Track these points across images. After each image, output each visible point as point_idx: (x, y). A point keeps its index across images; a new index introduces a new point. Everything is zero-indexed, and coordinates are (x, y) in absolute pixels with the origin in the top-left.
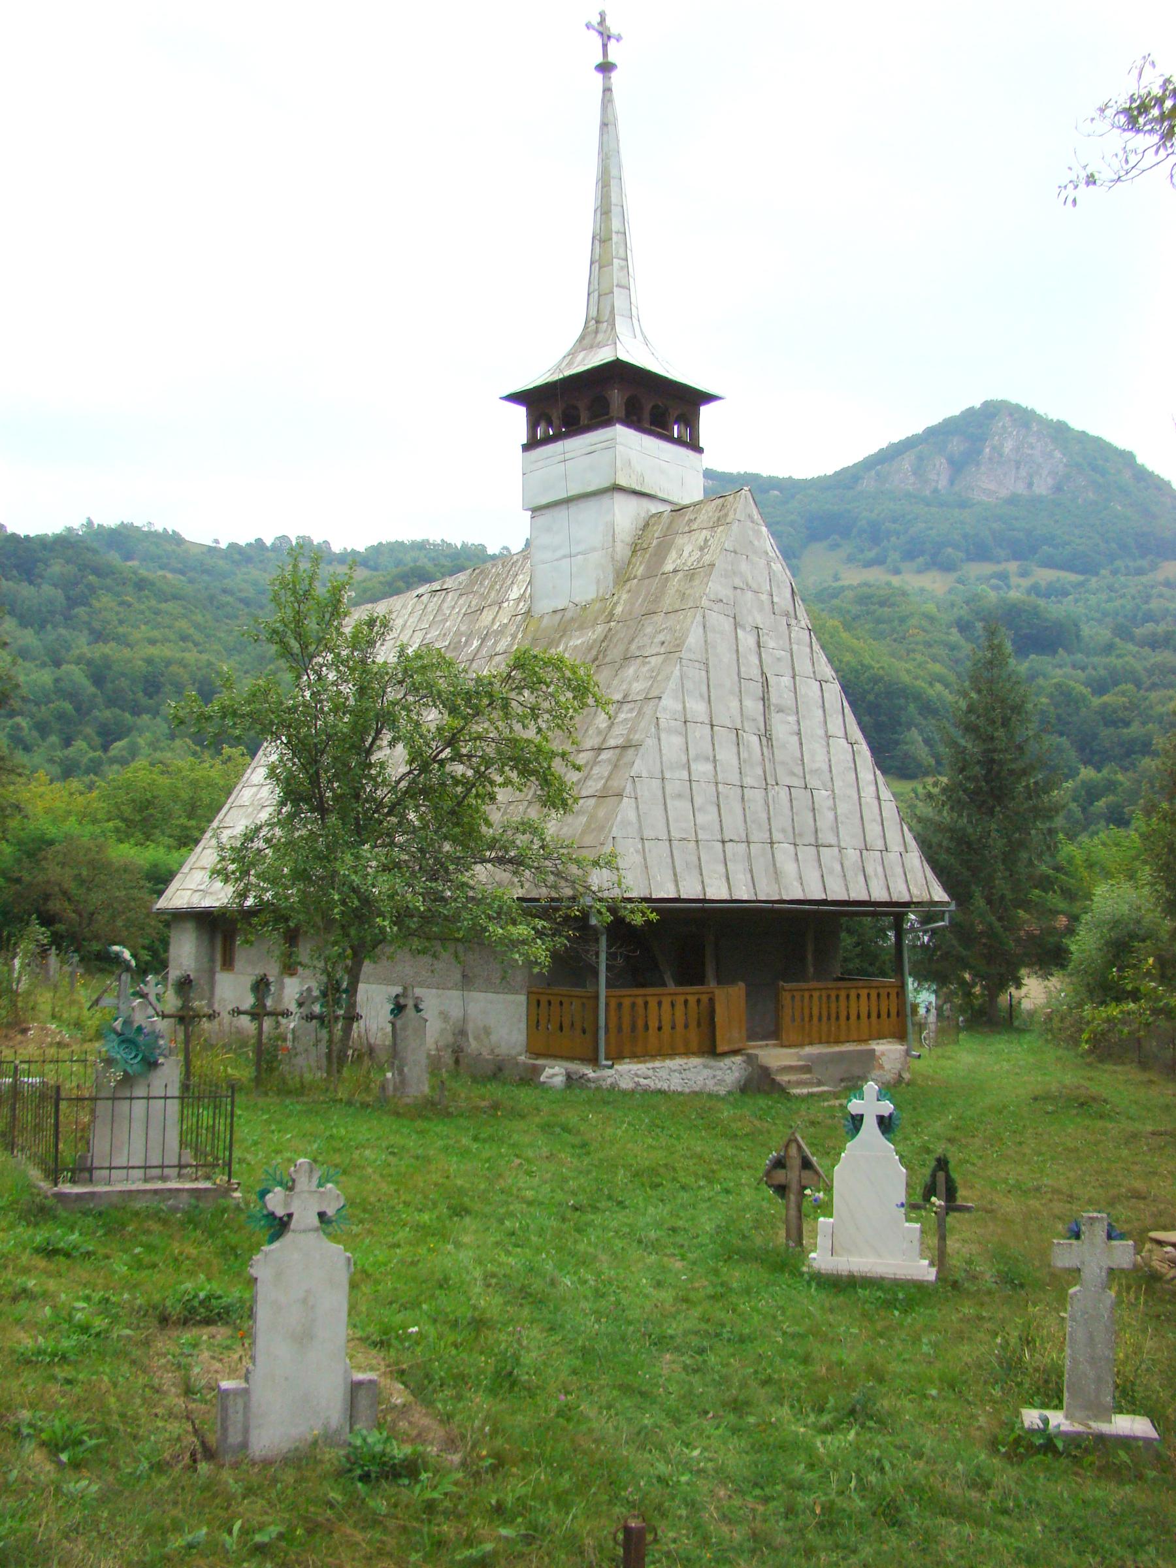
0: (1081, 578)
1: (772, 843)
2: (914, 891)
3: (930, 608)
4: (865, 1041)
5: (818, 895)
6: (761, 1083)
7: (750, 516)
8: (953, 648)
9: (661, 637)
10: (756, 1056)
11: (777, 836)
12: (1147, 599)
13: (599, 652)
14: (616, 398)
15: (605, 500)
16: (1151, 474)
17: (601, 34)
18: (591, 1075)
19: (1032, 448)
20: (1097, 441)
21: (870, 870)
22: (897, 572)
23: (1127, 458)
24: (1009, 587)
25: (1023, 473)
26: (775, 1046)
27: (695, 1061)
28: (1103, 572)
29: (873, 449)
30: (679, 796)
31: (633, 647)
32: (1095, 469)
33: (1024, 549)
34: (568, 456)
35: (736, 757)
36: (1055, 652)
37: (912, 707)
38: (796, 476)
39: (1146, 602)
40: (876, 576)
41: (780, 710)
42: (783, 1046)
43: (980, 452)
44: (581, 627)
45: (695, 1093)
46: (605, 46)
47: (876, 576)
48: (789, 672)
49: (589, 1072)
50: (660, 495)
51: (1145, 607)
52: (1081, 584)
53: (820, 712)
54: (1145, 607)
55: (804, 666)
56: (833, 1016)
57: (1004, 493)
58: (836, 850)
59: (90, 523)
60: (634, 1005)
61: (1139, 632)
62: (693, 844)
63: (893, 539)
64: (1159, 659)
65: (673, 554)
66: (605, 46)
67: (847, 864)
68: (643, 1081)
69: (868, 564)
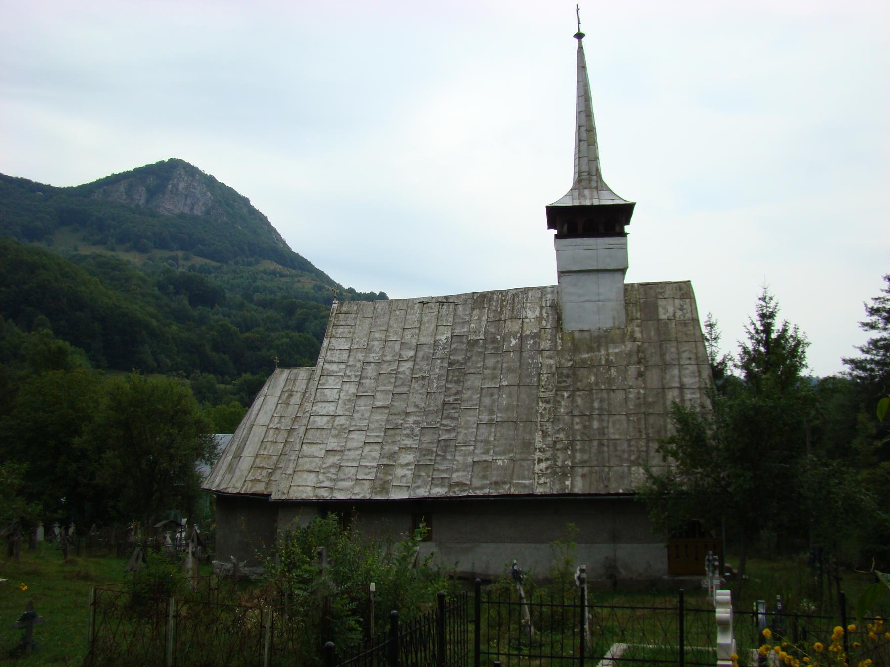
0: (219, 264)
3: (142, 274)
16: (257, 212)
20: (231, 189)
23: (246, 201)
25: (189, 201)
29: (103, 176)
36: (212, 307)
38: (53, 185)
40: (99, 250)
44: (613, 342)
47: (99, 250)
52: (219, 268)
57: (177, 211)
69: (95, 243)
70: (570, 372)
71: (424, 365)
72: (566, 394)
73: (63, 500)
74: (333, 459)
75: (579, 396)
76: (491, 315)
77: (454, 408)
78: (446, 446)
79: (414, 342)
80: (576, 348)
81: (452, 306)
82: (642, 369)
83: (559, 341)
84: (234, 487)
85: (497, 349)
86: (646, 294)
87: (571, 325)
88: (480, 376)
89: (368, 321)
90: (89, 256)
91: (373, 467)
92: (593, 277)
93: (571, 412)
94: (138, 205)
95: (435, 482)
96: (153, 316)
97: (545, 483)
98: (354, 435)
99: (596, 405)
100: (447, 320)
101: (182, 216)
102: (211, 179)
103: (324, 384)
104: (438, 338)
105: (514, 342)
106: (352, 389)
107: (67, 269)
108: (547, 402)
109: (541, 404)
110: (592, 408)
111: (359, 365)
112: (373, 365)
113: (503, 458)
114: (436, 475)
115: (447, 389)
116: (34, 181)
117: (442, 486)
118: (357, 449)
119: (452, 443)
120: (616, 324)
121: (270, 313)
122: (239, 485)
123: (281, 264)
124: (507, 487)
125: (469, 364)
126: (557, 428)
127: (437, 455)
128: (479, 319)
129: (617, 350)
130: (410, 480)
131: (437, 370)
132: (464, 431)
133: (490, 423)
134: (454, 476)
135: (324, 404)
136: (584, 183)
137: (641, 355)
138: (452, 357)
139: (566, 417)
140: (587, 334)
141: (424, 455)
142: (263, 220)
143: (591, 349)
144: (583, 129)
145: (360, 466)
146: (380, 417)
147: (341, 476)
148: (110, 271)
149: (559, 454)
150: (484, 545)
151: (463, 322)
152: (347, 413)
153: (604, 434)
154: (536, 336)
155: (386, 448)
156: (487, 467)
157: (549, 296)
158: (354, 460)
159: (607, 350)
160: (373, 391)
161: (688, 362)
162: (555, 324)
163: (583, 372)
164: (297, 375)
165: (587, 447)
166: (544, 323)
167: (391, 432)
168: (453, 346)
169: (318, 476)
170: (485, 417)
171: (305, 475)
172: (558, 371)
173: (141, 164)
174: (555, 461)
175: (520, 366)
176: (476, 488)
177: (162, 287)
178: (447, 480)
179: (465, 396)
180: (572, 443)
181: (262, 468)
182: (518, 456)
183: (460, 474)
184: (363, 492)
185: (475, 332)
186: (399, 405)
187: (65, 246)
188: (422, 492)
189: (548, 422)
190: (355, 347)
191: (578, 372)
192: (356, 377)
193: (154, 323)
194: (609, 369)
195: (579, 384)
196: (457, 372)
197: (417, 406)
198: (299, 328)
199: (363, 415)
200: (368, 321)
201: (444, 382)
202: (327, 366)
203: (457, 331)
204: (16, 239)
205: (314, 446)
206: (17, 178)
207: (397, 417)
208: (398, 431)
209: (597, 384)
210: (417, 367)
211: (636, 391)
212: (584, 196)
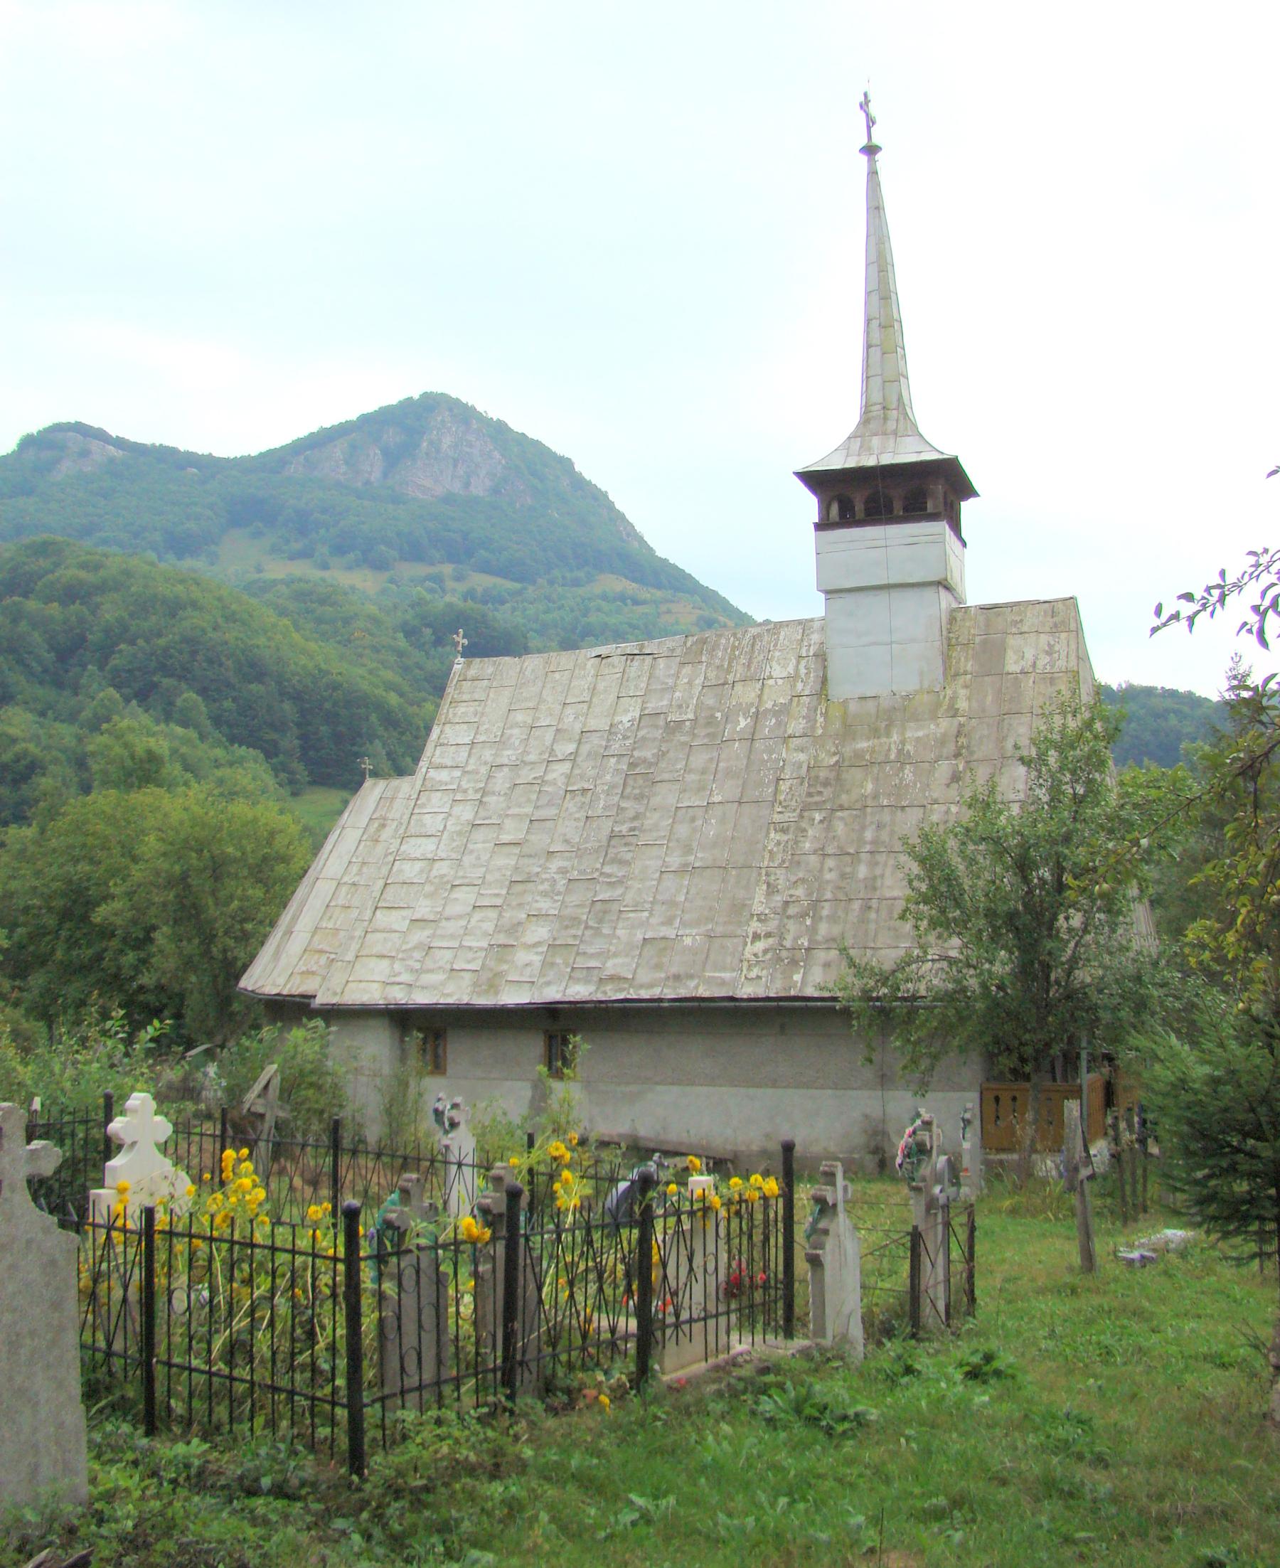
0: (518, 586)
3: (372, 609)
8: (401, 654)
15: (929, 593)
19: (471, 446)
20: (537, 444)
22: (325, 566)
24: (443, 590)
28: (540, 581)
29: (303, 432)
33: (461, 551)
37: (373, 718)
38: (217, 454)
39: (585, 616)
40: (301, 569)
44: (915, 718)
52: (519, 593)
59: (1240, 682)
63: (322, 531)
70: (832, 775)
71: (588, 768)
72: (818, 817)
74: (420, 935)
75: (842, 819)
76: (712, 674)
77: (626, 844)
78: (603, 911)
79: (578, 727)
80: (848, 730)
81: (649, 659)
82: (961, 768)
83: (820, 720)
84: (274, 985)
85: (711, 736)
86: (987, 625)
87: (838, 691)
88: (677, 786)
89: (507, 693)
90: (282, 581)
91: (481, 949)
92: (884, 595)
93: (822, 849)
94: (367, 483)
95: (577, 974)
96: (390, 687)
97: (759, 977)
98: (459, 894)
99: (868, 835)
100: (636, 687)
101: (449, 499)
103: (423, 806)
104: (617, 719)
105: (743, 723)
107: (234, 607)
108: (784, 831)
109: (772, 835)
110: (861, 841)
111: (484, 770)
112: (506, 769)
113: (694, 932)
114: (581, 962)
115: (621, 810)
117: (587, 981)
118: (460, 917)
119: (615, 907)
120: (926, 685)
122: (281, 981)
124: (692, 984)
125: (663, 765)
126: (793, 879)
127: (586, 928)
128: (690, 683)
129: (920, 734)
130: (537, 972)
131: (608, 777)
132: (637, 885)
133: (683, 870)
134: (610, 964)
135: (420, 840)
136: (872, 426)
137: (962, 740)
138: (636, 754)
139: (813, 858)
140: (871, 705)
141: (567, 927)
142: (598, 498)
143: (875, 733)
144: (875, 324)
145: (461, 946)
146: (505, 861)
147: (429, 964)
148: (314, 606)
149: (792, 926)
150: (659, 1088)
151: (663, 690)
152: (454, 856)
153: (875, 889)
154: (782, 711)
155: (507, 915)
156: (665, 949)
157: (815, 638)
158: (453, 937)
159: (903, 734)
160: (500, 816)
162: (818, 687)
163: (857, 774)
164: (397, 790)
165: (840, 913)
166: (800, 686)
167: (519, 887)
168: (641, 734)
169: (392, 965)
170: (675, 861)
171: (373, 962)
172: (811, 778)
173: (370, 407)
174: (782, 938)
175: (747, 766)
176: (641, 986)
177: (410, 632)
178: (596, 972)
179: (648, 823)
180: (816, 904)
181: (321, 952)
182: (720, 930)
183: (619, 960)
184: (458, 993)
185: (680, 706)
186: (539, 840)
187: (240, 568)
189: (780, 866)
190: (481, 738)
191: (844, 776)
192: (476, 791)
193: (393, 699)
194: (902, 769)
195: (844, 797)
196: (640, 777)
197: (567, 841)
199: (478, 858)
200: (507, 693)
201: (617, 798)
202: (432, 773)
203: (651, 706)
204: (152, 556)
205: (394, 912)
207: (531, 861)
208: (530, 886)
209: (875, 796)
210: (577, 771)
211: (943, 808)
212: (869, 449)
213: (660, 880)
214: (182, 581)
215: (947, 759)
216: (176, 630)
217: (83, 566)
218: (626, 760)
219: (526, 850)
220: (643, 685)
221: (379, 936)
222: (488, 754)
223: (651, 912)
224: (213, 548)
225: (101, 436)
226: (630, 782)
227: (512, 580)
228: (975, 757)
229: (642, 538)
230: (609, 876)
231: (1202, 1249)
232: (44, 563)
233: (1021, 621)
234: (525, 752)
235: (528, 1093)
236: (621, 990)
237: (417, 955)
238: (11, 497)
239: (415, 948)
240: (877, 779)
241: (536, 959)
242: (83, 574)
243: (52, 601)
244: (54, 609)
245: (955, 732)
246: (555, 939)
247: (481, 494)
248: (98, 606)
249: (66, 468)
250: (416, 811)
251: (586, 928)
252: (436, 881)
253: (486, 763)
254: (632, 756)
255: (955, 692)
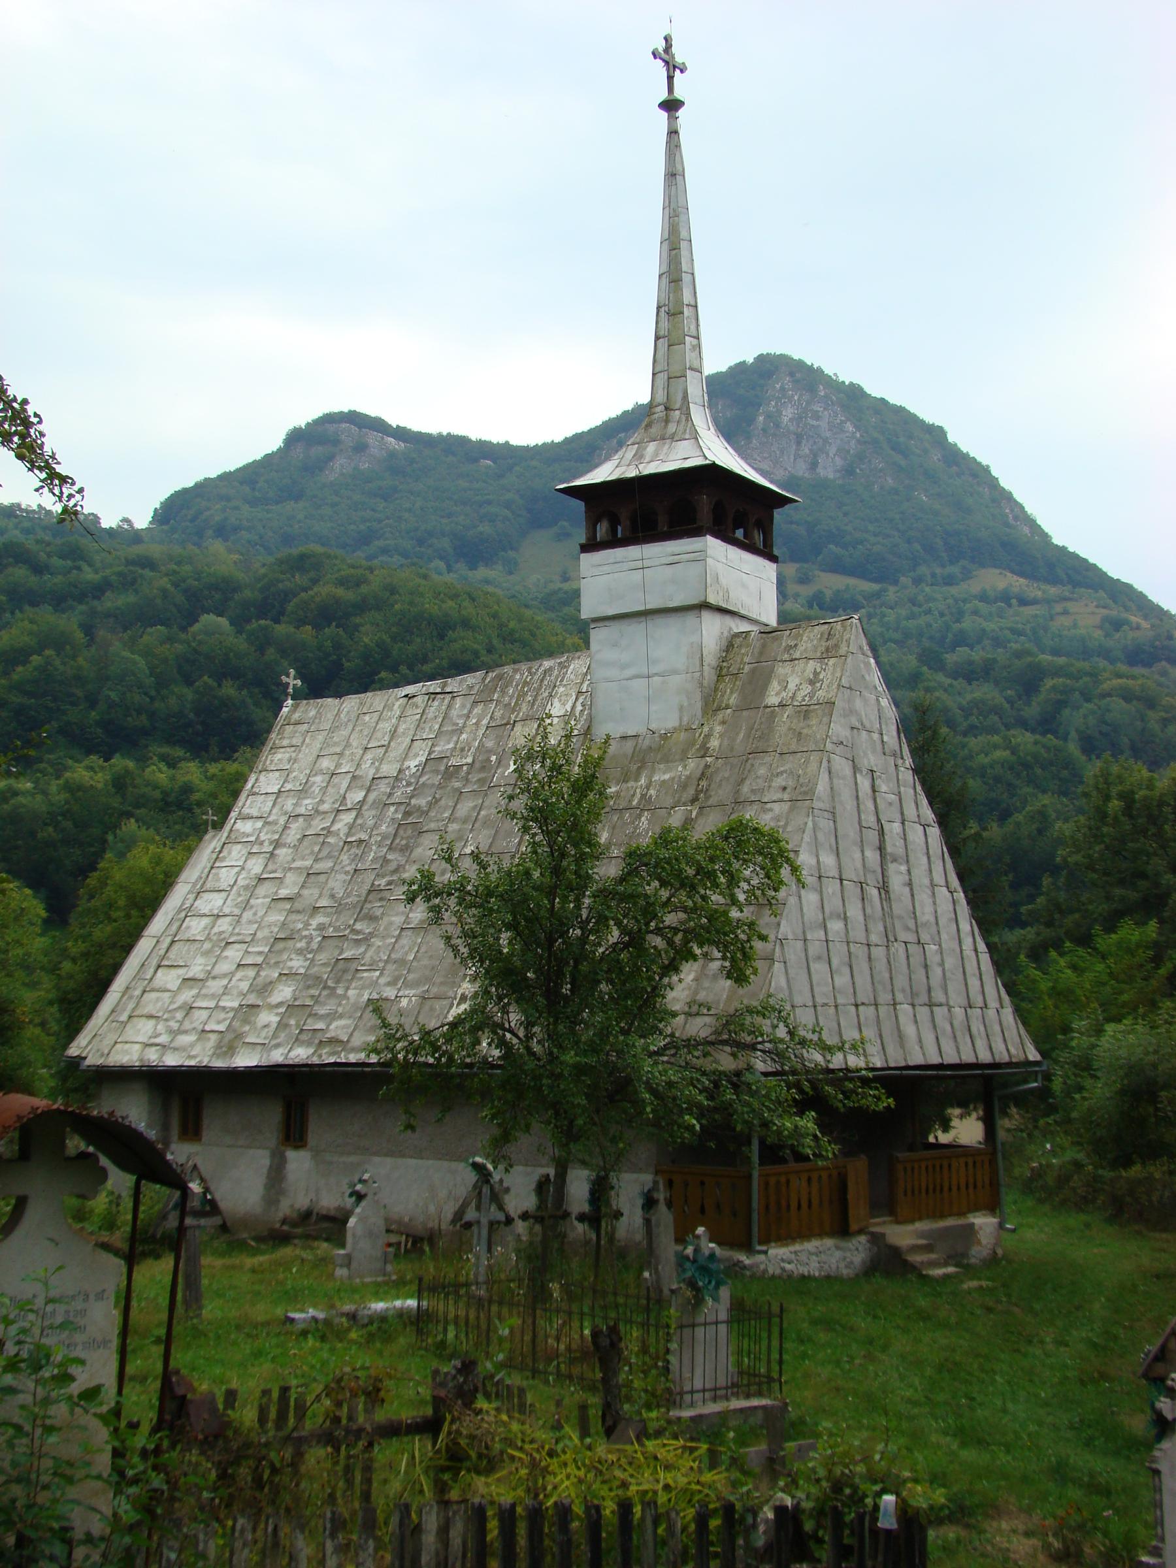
0: (875, 587)
1: (895, 1004)
2: (1013, 1051)
4: (962, 1214)
5: (935, 1060)
6: (889, 1263)
7: (861, 648)
9: (780, 781)
10: (883, 1235)
11: (900, 997)
12: (959, 616)
13: (698, 792)
14: (704, 503)
15: (691, 619)
16: (966, 457)
17: (667, 63)
18: (747, 1262)
19: (818, 418)
20: (900, 411)
21: (974, 1029)
23: (936, 434)
25: (806, 450)
26: (891, 1222)
27: (829, 1242)
28: (903, 579)
29: (614, 411)
30: (819, 958)
31: (745, 789)
32: (896, 448)
34: (646, 563)
35: (861, 913)
38: (514, 442)
39: (958, 621)
41: (895, 860)
42: (898, 1222)
43: (751, 421)
44: (666, 760)
45: (828, 1277)
46: (670, 79)
48: (898, 817)
49: (746, 1260)
50: (743, 612)
51: (956, 626)
52: (878, 595)
53: (925, 859)
54: (956, 626)
55: (910, 811)
56: (938, 1188)
58: (945, 1009)
60: (778, 1182)
61: (951, 658)
62: (832, 1010)
64: (977, 695)
65: (775, 685)
66: (670, 79)
67: (956, 1023)
68: (788, 1267)
73: (1048, 1146)
74: (187, 995)
77: (381, 899)
78: (344, 970)
81: (448, 697)
82: (694, 814)
89: (321, 737)
91: (232, 1009)
95: (304, 1037)
102: (854, 393)
106: (256, 866)
107: (512, 624)
112: (301, 819)
113: (412, 992)
115: (386, 861)
116: (474, 437)
117: (308, 1044)
119: (354, 966)
121: (983, 692)
123: (1021, 574)
129: (667, 777)
137: (704, 783)
140: (630, 744)
142: (979, 474)
146: (276, 917)
150: (377, 1159)
155: (263, 974)
161: (779, 796)
167: (281, 945)
182: (435, 990)
183: (342, 1022)
186: (310, 893)
188: (277, 1056)
190: (288, 786)
198: (1047, 724)
199: (255, 914)
200: (321, 737)
206: (440, 435)
208: (290, 943)
210: (359, 821)
213: (398, 937)
214: (454, 597)
215: (684, 804)
216: (443, 654)
217: (342, 582)
218: (402, 808)
219: (298, 905)
220: (437, 727)
221: (154, 995)
222: (289, 804)
223: (383, 970)
224: (511, 553)
225: (378, 425)
226: (401, 832)
227: (870, 580)
228: (709, 803)
229: (1034, 521)
230: (358, 932)
231: (1047, 1355)
232: (299, 579)
233: (796, 645)
234: (322, 801)
235: (267, 1162)
236: (338, 1053)
237: (179, 1015)
238: (277, 503)
239: (179, 1008)
240: (614, 828)
241: (275, 1019)
242: (340, 592)
243: (305, 624)
244: (307, 633)
245: (698, 773)
246: (295, 999)
247: (831, 476)
248: (356, 627)
249: (341, 465)
250: (217, 865)
251: (325, 988)
252: (215, 938)
253: (286, 813)
254: (409, 804)
255: (711, 729)
